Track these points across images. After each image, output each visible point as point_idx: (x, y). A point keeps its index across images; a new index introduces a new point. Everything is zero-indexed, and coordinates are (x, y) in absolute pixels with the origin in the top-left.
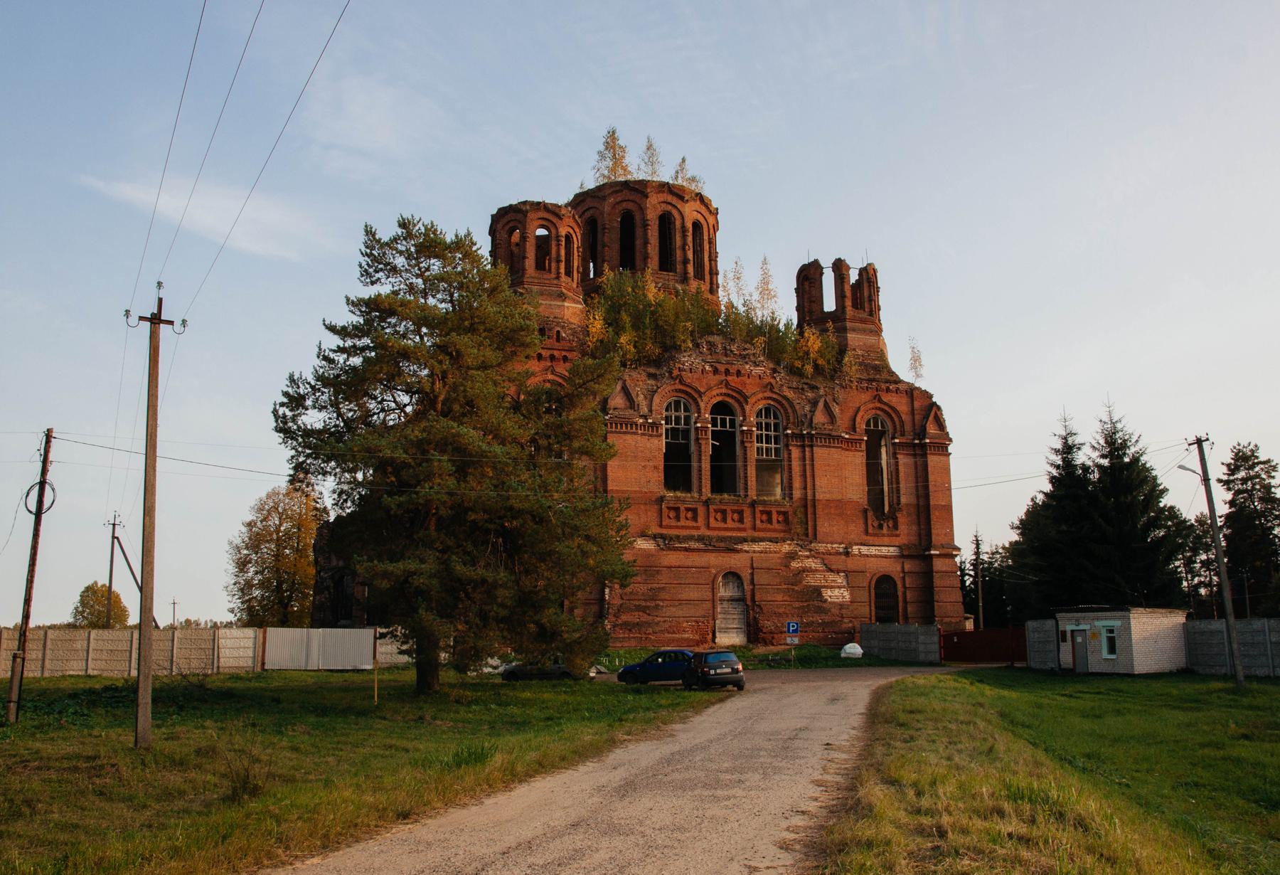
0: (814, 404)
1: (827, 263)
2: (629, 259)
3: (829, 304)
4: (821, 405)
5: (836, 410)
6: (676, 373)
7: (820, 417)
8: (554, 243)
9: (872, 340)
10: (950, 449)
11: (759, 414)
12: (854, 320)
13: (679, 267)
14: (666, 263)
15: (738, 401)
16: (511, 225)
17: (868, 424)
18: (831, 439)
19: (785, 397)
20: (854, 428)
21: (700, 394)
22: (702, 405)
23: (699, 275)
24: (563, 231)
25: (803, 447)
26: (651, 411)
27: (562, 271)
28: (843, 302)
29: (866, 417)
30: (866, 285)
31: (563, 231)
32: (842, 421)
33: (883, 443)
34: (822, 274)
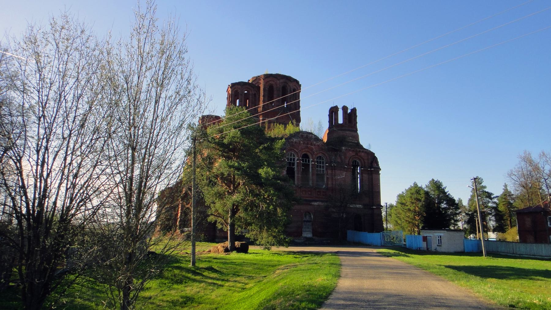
1: (340, 107)
3: (340, 121)
9: (353, 133)
10: (380, 172)
15: (311, 153)
17: (353, 163)
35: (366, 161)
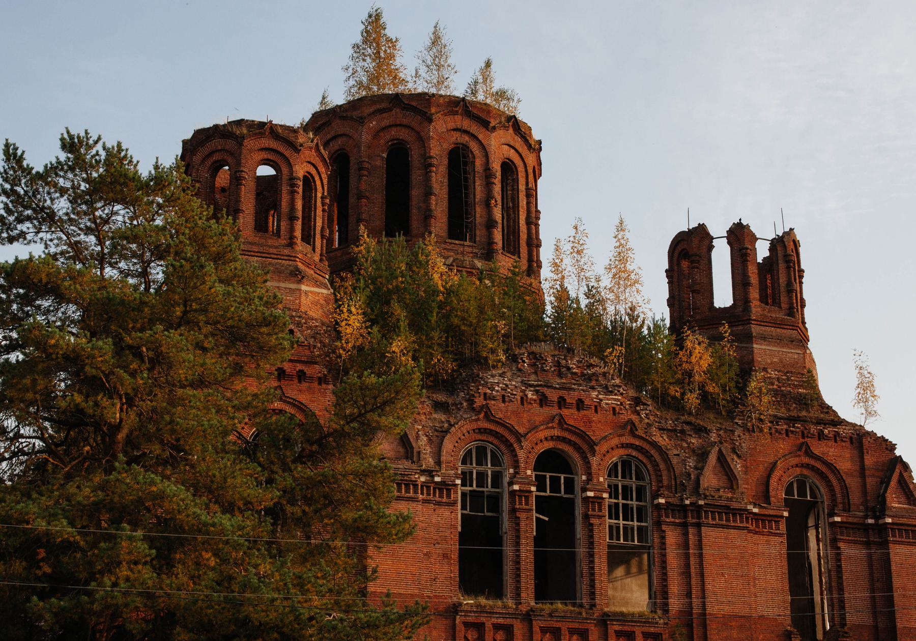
0: (702, 456)
1: (718, 229)
2: (399, 219)
4: (713, 458)
5: (738, 466)
6: (479, 401)
7: (710, 479)
8: (285, 189)
9: (791, 354)
11: (612, 472)
12: (762, 322)
13: (480, 233)
14: (458, 227)
15: (578, 449)
16: (216, 157)
17: (789, 491)
18: (729, 514)
19: (654, 445)
20: (766, 497)
21: (519, 437)
22: (521, 454)
23: (511, 247)
24: (300, 171)
25: (684, 525)
26: (438, 463)
27: (298, 233)
28: (746, 293)
29: (787, 479)
30: (782, 266)
31: (300, 171)
32: (747, 485)
33: (811, 522)
34: (711, 247)
35: (853, 483)
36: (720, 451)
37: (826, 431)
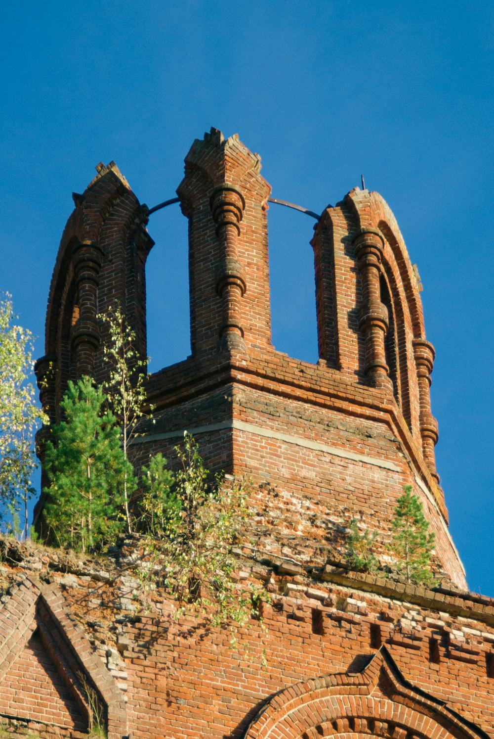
1: (155, 180)
36: (42, 606)
37: (457, 636)
